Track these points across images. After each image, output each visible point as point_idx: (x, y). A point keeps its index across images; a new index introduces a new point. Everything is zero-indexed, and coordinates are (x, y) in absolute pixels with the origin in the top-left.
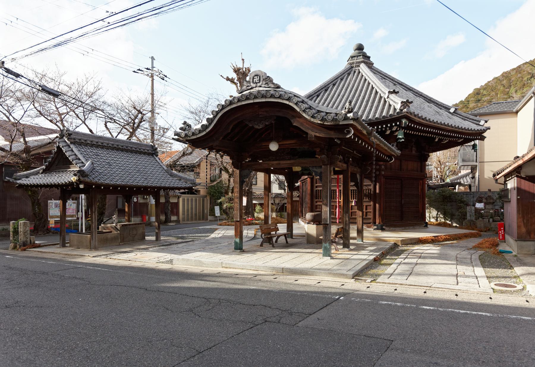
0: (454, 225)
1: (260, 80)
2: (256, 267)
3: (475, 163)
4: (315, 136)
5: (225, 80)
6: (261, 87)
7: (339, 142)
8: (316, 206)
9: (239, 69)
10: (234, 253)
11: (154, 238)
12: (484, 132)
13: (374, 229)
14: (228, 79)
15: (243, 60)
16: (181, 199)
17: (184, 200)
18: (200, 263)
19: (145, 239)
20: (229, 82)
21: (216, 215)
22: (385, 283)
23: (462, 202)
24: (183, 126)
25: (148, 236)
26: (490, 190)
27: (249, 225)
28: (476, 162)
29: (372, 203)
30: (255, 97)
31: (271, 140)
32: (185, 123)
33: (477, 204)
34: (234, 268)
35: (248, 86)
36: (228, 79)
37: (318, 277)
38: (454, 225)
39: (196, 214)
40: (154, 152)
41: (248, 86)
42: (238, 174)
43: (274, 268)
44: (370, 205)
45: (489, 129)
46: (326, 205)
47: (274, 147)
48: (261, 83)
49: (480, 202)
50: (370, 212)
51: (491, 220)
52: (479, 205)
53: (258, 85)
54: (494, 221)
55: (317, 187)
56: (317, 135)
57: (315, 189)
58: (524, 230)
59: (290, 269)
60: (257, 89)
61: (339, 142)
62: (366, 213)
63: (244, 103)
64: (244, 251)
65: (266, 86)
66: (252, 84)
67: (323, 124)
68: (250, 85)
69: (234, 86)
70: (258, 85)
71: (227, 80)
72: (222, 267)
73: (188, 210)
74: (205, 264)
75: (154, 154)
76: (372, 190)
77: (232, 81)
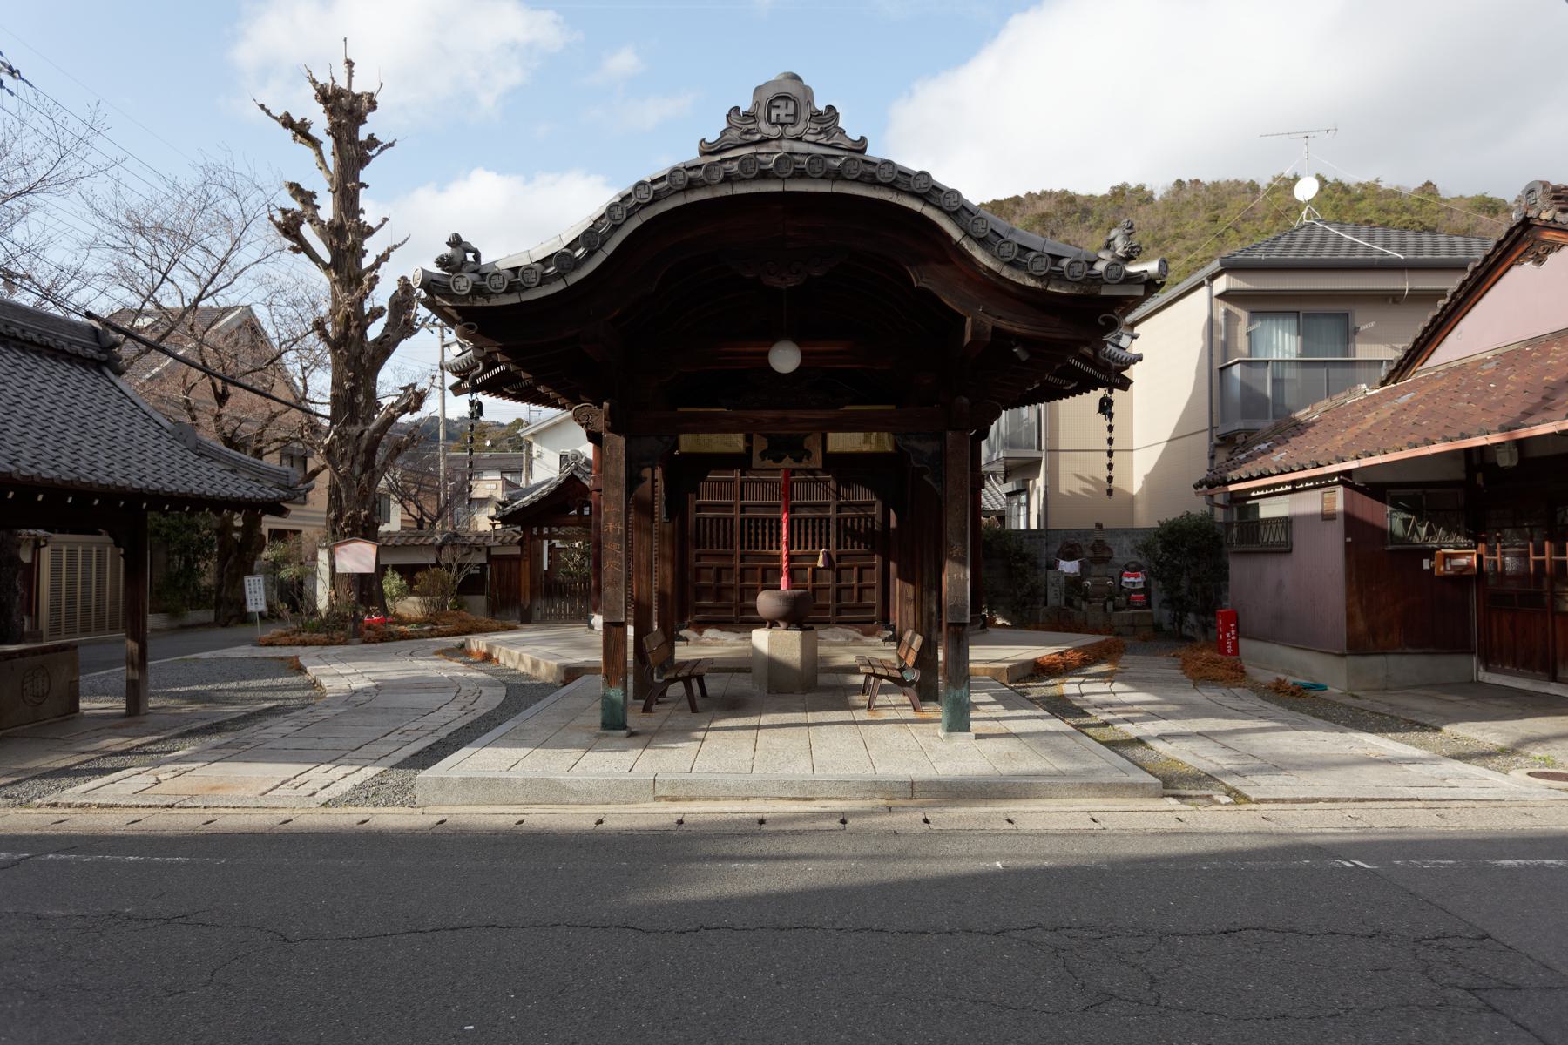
0: (1000, 621)
1: (795, 115)
2: (802, 786)
3: (1034, 454)
4: (994, 328)
5: (278, 126)
6: (799, 139)
7: (1024, 356)
8: (698, 569)
9: (339, 94)
10: (604, 740)
11: (119, 705)
12: (1127, 368)
13: (885, 640)
14: (287, 122)
15: (350, 63)
16: (46, 553)
17: (56, 555)
18: (552, 791)
19: (77, 709)
20: (289, 133)
21: (251, 608)
22: (1283, 801)
23: (1024, 558)
24: (448, 250)
25: (94, 693)
26: (1099, 525)
27: (382, 641)
28: (1040, 449)
29: (877, 560)
30: (800, 174)
31: (773, 338)
32: (456, 242)
33: (1062, 562)
34: (707, 799)
35: (748, 132)
36: (287, 122)
37: (1048, 801)
38: (1000, 621)
39: (86, 609)
40: (104, 357)
41: (748, 132)
42: (621, 454)
43: (876, 787)
44: (872, 567)
45: (1140, 359)
46: (962, 562)
47: (785, 359)
48: (799, 129)
49: (1070, 557)
50: (872, 587)
51: (1110, 605)
52: (1069, 567)
53: (791, 131)
54: (1116, 609)
55: (699, 508)
56: (1003, 324)
57: (693, 516)
58: (1361, 625)
59: (939, 783)
60: (786, 146)
61: (1024, 356)
62: (860, 589)
63: (741, 190)
64: (632, 734)
65: (822, 139)
66: (764, 126)
67: (1044, 291)
68: (759, 131)
69: (310, 152)
70: (791, 131)
71: (285, 125)
72: (657, 799)
73: (71, 590)
74: (575, 793)
75: (106, 363)
76: (879, 518)
77: (301, 130)
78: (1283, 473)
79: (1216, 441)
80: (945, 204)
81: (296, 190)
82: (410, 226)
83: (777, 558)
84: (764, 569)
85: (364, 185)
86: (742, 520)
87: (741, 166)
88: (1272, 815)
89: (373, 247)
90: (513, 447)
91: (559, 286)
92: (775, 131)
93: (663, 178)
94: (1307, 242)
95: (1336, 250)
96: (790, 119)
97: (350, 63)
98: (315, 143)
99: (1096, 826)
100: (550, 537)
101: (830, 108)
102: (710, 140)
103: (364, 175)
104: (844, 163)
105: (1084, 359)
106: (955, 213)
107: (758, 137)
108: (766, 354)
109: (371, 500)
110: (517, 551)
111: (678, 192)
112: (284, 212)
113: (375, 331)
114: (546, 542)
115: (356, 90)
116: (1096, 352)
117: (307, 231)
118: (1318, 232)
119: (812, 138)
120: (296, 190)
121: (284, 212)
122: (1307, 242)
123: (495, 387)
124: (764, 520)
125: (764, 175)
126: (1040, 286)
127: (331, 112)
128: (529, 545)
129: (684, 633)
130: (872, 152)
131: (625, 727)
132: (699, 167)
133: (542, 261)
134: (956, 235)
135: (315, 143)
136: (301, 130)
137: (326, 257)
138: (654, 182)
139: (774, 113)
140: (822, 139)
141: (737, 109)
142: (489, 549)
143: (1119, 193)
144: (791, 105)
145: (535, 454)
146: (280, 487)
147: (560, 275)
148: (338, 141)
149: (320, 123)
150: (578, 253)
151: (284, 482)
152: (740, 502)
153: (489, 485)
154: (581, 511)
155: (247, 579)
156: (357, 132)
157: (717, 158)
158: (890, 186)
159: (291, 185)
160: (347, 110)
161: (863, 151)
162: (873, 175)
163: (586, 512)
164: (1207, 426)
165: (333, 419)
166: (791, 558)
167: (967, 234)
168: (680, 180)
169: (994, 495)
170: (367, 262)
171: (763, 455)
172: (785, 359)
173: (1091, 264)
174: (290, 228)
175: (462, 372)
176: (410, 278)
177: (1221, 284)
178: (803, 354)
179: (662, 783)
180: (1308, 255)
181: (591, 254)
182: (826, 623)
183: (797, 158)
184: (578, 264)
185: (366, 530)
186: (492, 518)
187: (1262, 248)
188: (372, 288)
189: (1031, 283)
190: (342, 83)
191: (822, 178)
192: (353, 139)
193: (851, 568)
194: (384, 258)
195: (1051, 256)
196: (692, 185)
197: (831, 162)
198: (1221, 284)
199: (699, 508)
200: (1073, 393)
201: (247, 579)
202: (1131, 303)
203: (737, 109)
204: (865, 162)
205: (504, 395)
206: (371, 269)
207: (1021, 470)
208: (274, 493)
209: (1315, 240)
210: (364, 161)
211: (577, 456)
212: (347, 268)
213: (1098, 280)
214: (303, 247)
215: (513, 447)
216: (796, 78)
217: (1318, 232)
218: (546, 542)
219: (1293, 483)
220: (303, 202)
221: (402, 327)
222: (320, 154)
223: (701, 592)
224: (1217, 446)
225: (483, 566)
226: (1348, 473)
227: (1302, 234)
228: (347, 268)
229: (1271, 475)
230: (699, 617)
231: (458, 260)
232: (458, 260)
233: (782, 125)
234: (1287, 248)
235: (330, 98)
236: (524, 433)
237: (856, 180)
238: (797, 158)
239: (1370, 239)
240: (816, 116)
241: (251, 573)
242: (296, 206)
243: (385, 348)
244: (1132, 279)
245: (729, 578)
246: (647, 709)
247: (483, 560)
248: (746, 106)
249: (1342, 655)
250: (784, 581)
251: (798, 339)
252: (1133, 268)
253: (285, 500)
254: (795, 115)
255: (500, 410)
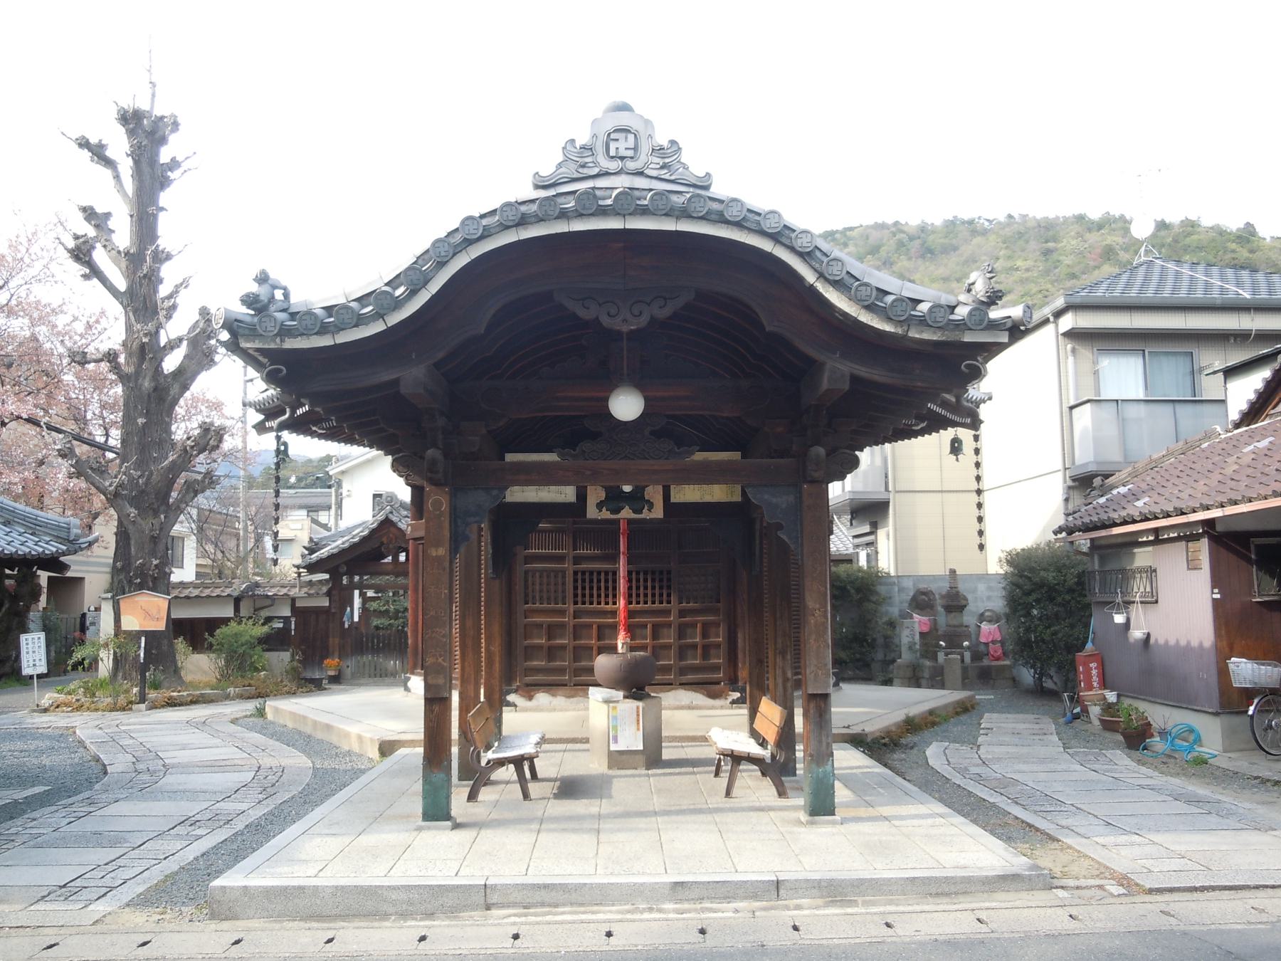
1: (635, 149)
6: (640, 173)
13: (733, 702)
14: (84, 144)
15: (153, 84)
20: (86, 154)
30: (644, 212)
31: (611, 382)
32: (263, 279)
36: (84, 144)
41: (583, 166)
45: (990, 399)
50: (718, 646)
55: (528, 559)
57: (520, 568)
64: (457, 826)
65: (664, 173)
68: (596, 164)
69: (108, 173)
70: (631, 165)
71: (81, 145)
77: (98, 153)
78: (1147, 519)
79: (1070, 483)
80: (798, 244)
81: (89, 214)
82: (206, 280)
83: (614, 613)
84: (600, 627)
85: (162, 209)
86: (575, 573)
87: (578, 201)
88: (1172, 908)
89: (169, 275)
90: (321, 479)
91: (377, 327)
92: (614, 166)
93: (493, 212)
94: (1147, 279)
95: (1191, 289)
96: (630, 153)
97: (153, 84)
98: (109, 163)
99: (984, 928)
100: (362, 587)
101: (673, 142)
102: (544, 173)
103: (164, 198)
104: (690, 199)
105: (945, 404)
106: (809, 253)
107: (596, 171)
108: (606, 399)
109: (161, 547)
110: (325, 602)
111: (508, 227)
112: (76, 237)
113: (171, 363)
114: (357, 593)
115: (158, 112)
116: (958, 398)
117: (100, 256)
118: (1157, 270)
119: (654, 173)
120: (89, 214)
121: (76, 237)
122: (1147, 279)
123: (300, 426)
124: (599, 573)
125: (603, 212)
126: (900, 331)
127: (131, 133)
128: (341, 597)
129: (511, 698)
130: (717, 190)
131: (448, 817)
132: (533, 201)
133: (358, 300)
134: (810, 277)
135: (109, 163)
136: (98, 153)
137: (121, 284)
138: (483, 216)
139: (613, 146)
140: (664, 173)
141: (573, 141)
142: (293, 600)
143: (951, 226)
144: (631, 137)
145: (345, 493)
146: (58, 539)
147: (379, 315)
148: (137, 163)
149: (119, 145)
150: (398, 292)
151: (63, 535)
152: (572, 553)
153: (295, 526)
154: (396, 558)
155: (23, 637)
156: (157, 154)
157: (552, 192)
158: (739, 225)
159: (84, 209)
160: (146, 132)
161: (707, 188)
162: (721, 214)
163: (402, 557)
164: (1060, 466)
165: (123, 456)
166: (631, 614)
167: (821, 276)
168: (512, 216)
169: (842, 539)
170: (163, 291)
171: (600, 506)
172: (626, 406)
173: (952, 308)
174: (81, 253)
175: (270, 412)
176: (213, 311)
177: (1067, 322)
178: (648, 401)
179: (494, 887)
180: (1150, 293)
181: (413, 293)
182: (669, 685)
183: (637, 193)
184: (398, 304)
185: (157, 581)
186: (298, 567)
187: (1104, 286)
188: (168, 317)
189: (888, 328)
190: (144, 105)
191: (666, 215)
192: (153, 161)
193: (694, 625)
194: (184, 284)
195: (878, 289)
196: (523, 221)
197: (674, 198)
198: (1067, 322)
199: (528, 559)
200: (922, 433)
201: (23, 637)
202: (992, 350)
203: (573, 141)
204: (710, 198)
205: (313, 434)
206: (170, 297)
207: (871, 512)
208: (52, 548)
209: (1155, 278)
210: (164, 183)
211: (391, 498)
212: (143, 301)
213: (961, 326)
214: (94, 272)
215: (321, 479)
216: (624, 108)
217: (1157, 270)
218: (357, 593)
219: (1156, 531)
220: (97, 226)
221: (201, 357)
222: (117, 177)
223: (530, 652)
224: (1070, 488)
225: (286, 620)
226: (1210, 523)
227: (1142, 270)
228: (143, 301)
229: (1134, 522)
230: (529, 679)
231: (264, 298)
232: (264, 298)
233: (622, 158)
234: (1128, 285)
235: (131, 120)
236: (333, 470)
237: (702, 218)
238: (637, 193)
239: (1239, 284)
240: (658, 151)
241: (26, 631)
242: (91, 232)
243: (184, 377)
244: (994, 326)
245: (562, 636)
246: (472, 797)
247: (287, 612)
248: (583, 139)
249: (1216, 714)
250: (621, 641)
251: (639, 383)
252: (995, 314)
253: (64, 554)
254: (635, 149)
255: (305, 447)
